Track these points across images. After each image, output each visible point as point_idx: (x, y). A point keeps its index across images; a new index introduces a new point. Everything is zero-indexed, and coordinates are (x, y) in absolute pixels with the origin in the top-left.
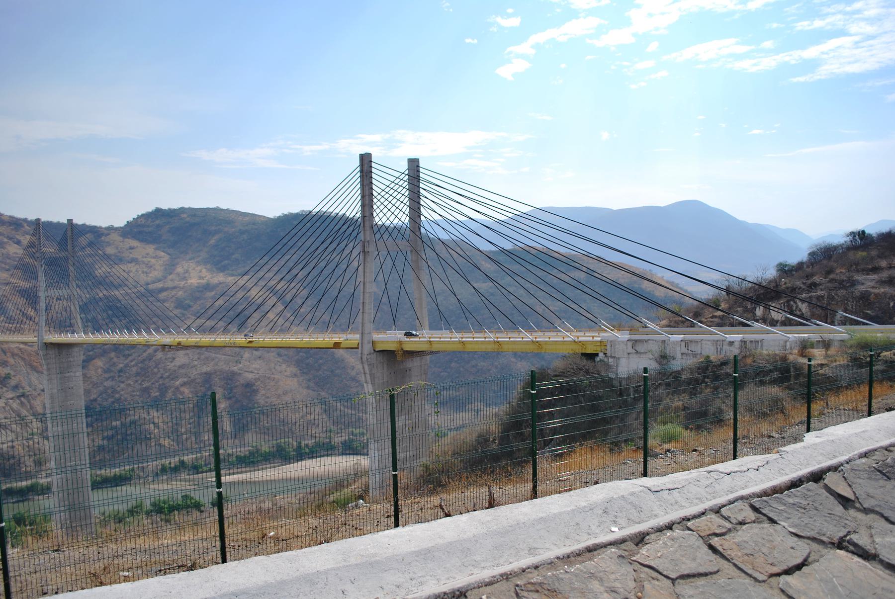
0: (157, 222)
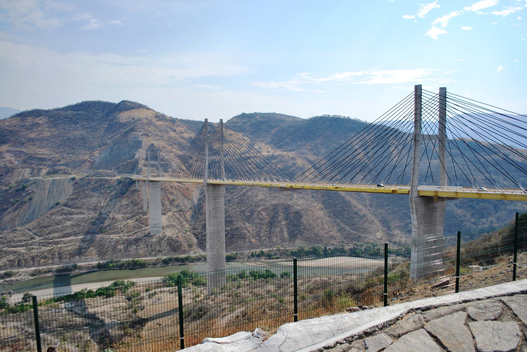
0: (243, 121)
